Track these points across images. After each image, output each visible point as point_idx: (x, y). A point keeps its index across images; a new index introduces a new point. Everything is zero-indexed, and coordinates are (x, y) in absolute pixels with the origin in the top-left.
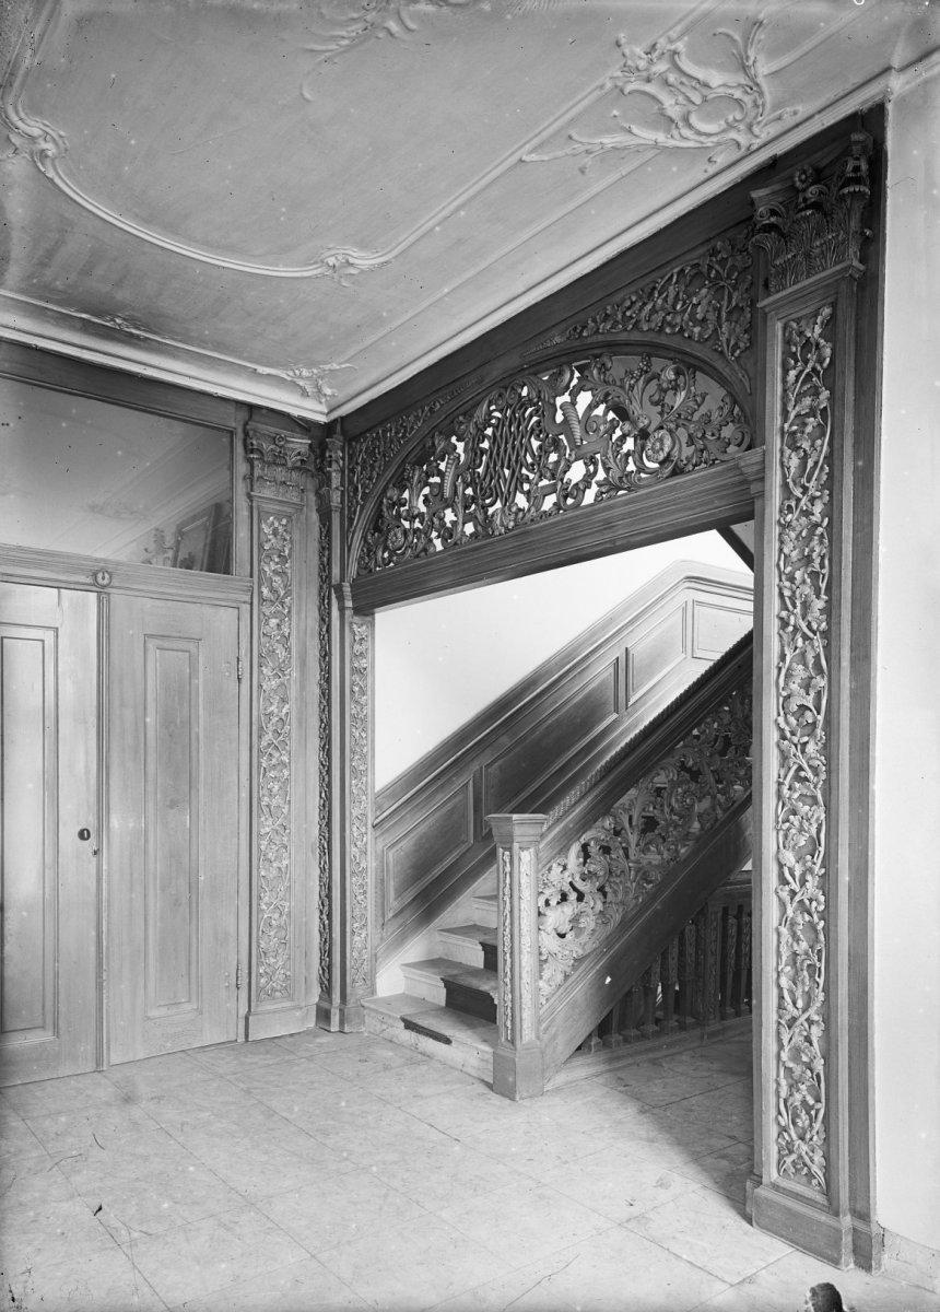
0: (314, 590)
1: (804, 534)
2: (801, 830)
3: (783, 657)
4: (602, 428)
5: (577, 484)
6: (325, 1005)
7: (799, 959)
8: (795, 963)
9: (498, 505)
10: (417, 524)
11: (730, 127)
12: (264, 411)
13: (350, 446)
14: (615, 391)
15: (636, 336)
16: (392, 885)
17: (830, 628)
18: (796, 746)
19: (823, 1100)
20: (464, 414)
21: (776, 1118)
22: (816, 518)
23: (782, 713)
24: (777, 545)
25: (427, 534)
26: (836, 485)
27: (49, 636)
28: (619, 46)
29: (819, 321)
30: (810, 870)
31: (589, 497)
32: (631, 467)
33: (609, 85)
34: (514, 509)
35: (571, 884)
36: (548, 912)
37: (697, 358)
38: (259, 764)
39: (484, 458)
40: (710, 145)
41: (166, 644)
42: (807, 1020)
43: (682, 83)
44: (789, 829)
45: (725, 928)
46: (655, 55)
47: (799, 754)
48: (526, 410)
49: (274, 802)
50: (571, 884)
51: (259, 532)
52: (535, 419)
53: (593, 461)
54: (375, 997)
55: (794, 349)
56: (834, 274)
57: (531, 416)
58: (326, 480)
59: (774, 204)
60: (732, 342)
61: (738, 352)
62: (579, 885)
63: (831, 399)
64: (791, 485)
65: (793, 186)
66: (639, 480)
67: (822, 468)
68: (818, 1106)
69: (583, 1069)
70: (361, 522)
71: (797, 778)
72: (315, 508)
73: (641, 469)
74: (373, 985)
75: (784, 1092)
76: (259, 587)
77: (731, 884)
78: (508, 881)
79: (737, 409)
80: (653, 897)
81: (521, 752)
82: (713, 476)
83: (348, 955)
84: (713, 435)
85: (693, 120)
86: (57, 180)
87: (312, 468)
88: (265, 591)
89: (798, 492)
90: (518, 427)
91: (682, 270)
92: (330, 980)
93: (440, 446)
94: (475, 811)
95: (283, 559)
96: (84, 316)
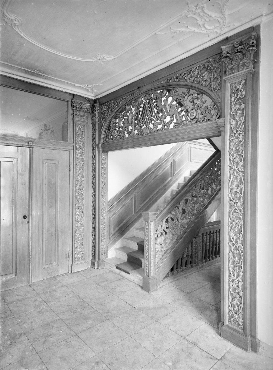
0: (91, 145)
1: (237, 143)
2: (236, 227)
3: (230, 177)
4: (175, 107)
5: (168, 122)
6: (93, 261)
7: (235, 263)
8: (234, 264)
9: (145, 126)
10: (121, 129)
11: (215, 28)
12: (77, 96)
13: (101, 106)
14: (179, 98)
15: (186, 83)
16: (112, 227)
17: (244, 171)
18: (234, 203)
19: (242, 303)
20: (135, 100)
21: (228, 307)
22: (241, 139)
23: (230, 193)
24: (229, 146)
25: (124, 133)
26: (246, 130)
27: (15, 160)
28: (188, 4)
29: (241, 84)
30: (239, 239)
31: (172, 126)
32: (184, 119)
33: (183, 15)
34: (149, 128)
35: (164, 230)
36: (158, 239)
37: (203, 91)
38: (75, 194)
39: (140, 113)
40: (209, 32)
41: (49, 162)
42: (238, 280)
43: (204, 15)
44: (232, 226)
45: (203, 239)
46: (197, 7)
47: (235, 205)
48: (153, 100)
49: (80, 205)
50: (164, 230)
51: (76, 130)
52: (155, 103)
53: (173, 116)
54: (108, 258)
55: (234, 91)
56: (245, 72)
57: (154, 102)
58: (95, 115)
59: (228, 50)
60: (215, 88)
61: (216, 90)
62: (166, 230)
63: (245, 106)
64: (233, 129)
65: (234, 46)
66: (186, 123)
67: (242, 126)
68: (241, 305)
69: (167, 281)
70: (105, 127)
71: (235, 212)
72: (91, 123)
73: (187, 120)
74: (107, 255)
75: (231, 300)
76: (76, 145)
77: (204, 227)
78: (147, 231)
79: (215, 106)
80: (185, 232)
81: (146, 189)
82: (209, 124)
83: (100, 247)
84: (208, 112)
85: (206, 26)
86: (19, 32)
87: (90, 112)
88: (77, 146)
89: (235, 132)
90: (150, 105)
91: (200, 66)
92: (95, 254)
93: (128, 108)
94: (134, 205)
95: (82, 137)
96: (26, 69)
